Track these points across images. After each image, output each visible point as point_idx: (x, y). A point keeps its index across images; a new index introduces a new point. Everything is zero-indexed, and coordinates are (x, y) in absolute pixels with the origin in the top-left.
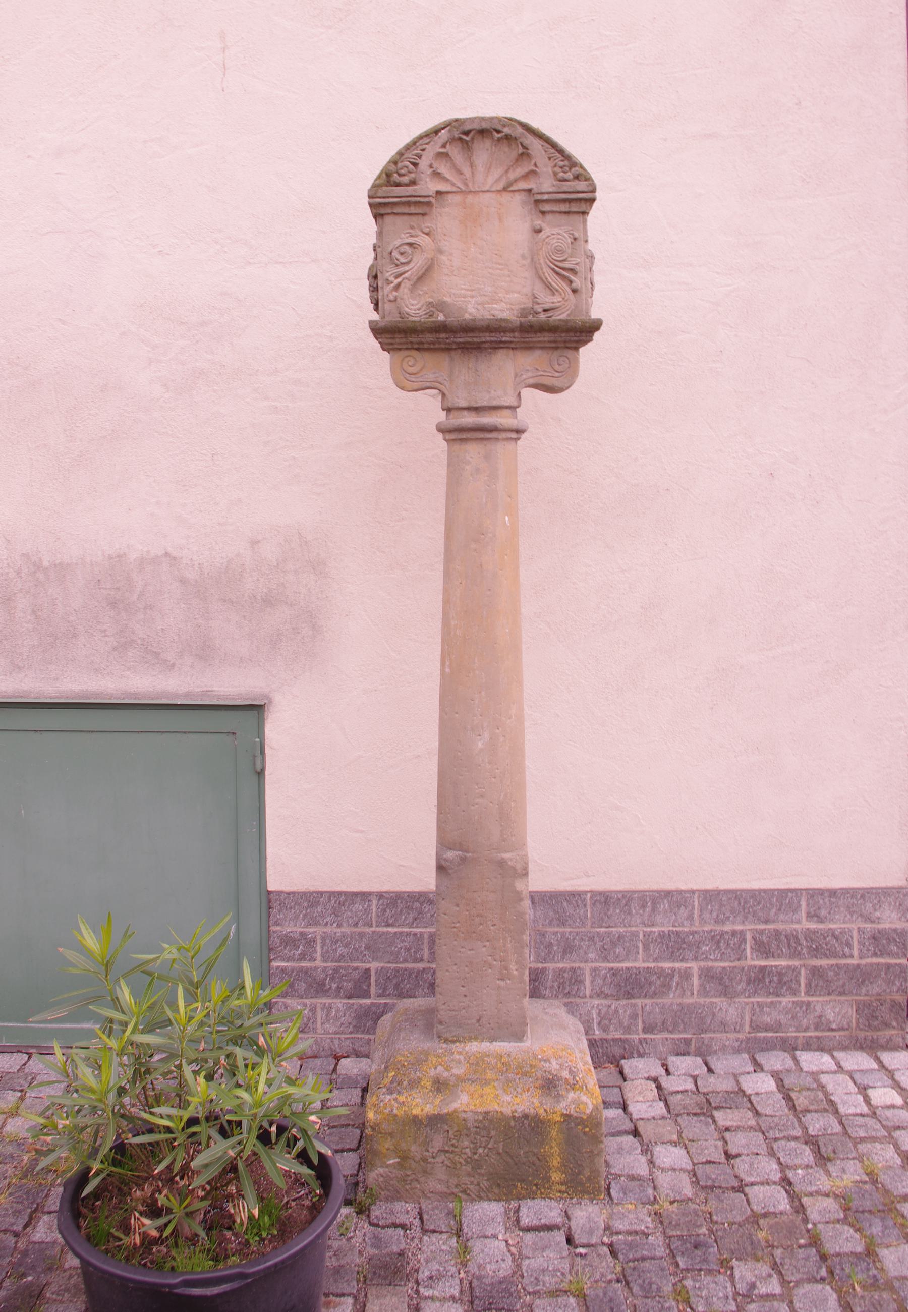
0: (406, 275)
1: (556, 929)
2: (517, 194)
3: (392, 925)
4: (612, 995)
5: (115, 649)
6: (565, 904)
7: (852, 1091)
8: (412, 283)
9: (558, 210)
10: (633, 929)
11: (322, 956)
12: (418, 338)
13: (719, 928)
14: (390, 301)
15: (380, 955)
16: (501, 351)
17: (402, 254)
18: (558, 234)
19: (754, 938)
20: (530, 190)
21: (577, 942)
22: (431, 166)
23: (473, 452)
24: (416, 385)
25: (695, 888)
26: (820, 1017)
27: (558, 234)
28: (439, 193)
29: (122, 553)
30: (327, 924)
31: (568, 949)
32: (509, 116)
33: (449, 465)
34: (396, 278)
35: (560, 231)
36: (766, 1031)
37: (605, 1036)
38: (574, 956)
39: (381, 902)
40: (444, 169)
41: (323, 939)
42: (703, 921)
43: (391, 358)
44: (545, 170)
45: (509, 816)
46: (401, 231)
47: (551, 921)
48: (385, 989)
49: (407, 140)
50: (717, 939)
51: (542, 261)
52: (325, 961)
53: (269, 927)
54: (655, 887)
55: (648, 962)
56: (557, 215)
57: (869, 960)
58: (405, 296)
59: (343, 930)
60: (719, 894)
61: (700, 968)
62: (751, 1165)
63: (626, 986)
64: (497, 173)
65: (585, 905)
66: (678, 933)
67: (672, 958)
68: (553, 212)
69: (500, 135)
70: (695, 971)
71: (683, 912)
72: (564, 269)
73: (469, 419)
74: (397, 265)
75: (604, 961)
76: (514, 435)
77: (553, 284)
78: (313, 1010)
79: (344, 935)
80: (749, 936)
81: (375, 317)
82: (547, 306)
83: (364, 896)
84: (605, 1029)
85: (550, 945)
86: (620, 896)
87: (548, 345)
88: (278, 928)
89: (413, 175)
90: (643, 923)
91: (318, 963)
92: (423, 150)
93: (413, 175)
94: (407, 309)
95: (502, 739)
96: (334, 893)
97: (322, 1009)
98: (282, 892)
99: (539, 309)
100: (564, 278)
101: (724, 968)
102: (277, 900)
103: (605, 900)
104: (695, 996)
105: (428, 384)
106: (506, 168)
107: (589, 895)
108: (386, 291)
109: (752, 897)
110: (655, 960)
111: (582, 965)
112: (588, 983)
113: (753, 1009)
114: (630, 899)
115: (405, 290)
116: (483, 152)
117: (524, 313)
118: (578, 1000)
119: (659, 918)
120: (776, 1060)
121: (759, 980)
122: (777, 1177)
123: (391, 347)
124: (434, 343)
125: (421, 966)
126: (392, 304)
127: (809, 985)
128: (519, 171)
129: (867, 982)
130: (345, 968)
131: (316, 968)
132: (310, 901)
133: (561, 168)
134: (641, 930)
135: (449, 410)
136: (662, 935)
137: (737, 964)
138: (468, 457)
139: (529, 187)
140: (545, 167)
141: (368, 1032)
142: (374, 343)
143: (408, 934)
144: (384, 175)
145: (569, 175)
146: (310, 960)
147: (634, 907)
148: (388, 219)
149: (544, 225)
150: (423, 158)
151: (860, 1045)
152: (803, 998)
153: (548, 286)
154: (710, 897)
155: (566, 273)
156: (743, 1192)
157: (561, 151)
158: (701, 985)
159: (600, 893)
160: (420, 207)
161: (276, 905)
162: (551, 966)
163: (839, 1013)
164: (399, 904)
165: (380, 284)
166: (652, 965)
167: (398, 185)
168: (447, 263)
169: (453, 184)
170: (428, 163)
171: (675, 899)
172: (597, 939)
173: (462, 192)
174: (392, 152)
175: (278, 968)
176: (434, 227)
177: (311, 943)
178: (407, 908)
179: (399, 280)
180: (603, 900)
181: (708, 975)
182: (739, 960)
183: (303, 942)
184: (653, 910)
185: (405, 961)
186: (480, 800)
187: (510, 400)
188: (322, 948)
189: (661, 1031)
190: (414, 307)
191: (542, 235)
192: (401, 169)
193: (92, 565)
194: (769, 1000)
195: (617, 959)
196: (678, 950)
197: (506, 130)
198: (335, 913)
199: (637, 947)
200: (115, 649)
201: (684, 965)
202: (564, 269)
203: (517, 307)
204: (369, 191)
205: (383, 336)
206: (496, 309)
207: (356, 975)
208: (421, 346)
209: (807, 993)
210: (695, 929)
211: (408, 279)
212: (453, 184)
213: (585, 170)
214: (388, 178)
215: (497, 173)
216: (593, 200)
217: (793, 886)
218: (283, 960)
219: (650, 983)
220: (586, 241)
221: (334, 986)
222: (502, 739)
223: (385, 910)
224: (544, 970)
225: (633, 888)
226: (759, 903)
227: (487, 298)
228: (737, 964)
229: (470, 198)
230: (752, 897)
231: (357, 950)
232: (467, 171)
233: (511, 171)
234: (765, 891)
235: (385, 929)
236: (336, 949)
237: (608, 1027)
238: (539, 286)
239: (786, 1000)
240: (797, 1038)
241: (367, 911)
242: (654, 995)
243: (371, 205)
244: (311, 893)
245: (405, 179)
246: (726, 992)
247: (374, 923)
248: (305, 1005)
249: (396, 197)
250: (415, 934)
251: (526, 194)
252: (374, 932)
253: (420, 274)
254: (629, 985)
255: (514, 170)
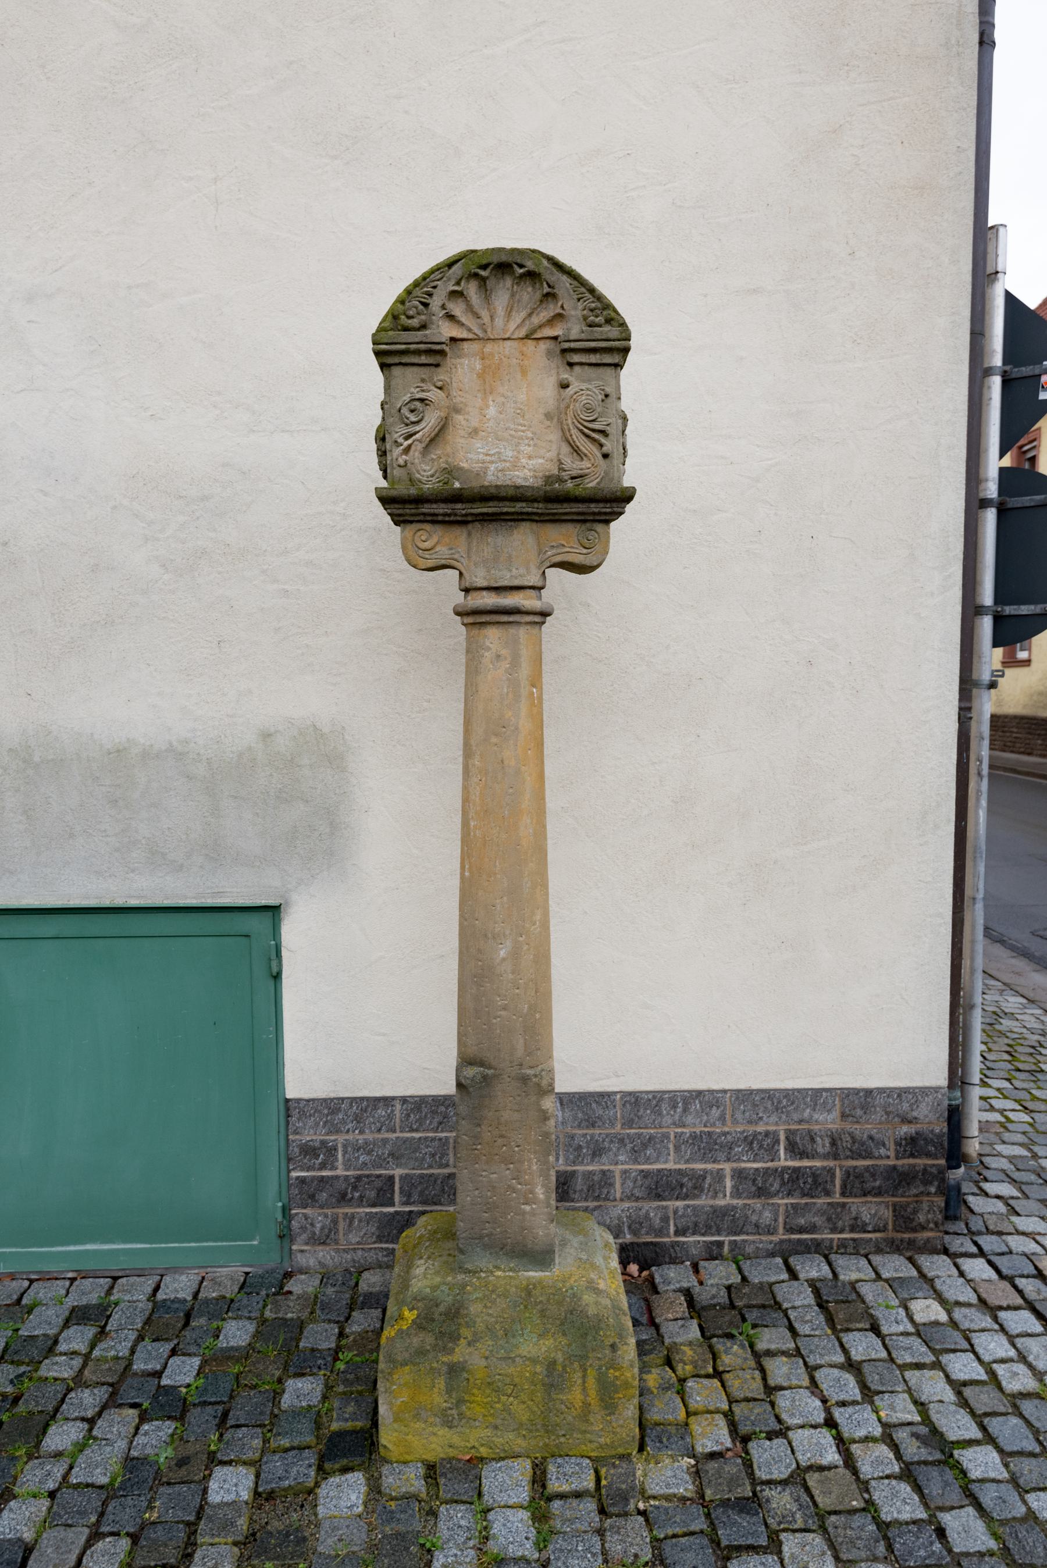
0: (417, 436)
1: (585, 1132)
2: (541, 343)
3: (417, 1130)
4: (642, 1198)
5: (117, 850)
6: (594, 1105)
7: (946, 1399)
8: (424, 445)
9: (588, 361)
10: (664, 1130)
11: (344, 1164)
12: (428, 507)
13: (751, 1129)
14: (399, 466)
15: (403, 1161)
16: (524, 524)
17: (412, 411)
18: (588, 389)
19: (787, 1138)
20: (555, 338)
21: (606, 1144)
22: (443, 307)
23: (493, 637)
24: (430, 563)
25: (727, 1087)
26: (856, 1219)
27: (588, 389)
28: (453, 340)
29: (272, 730)
30: (348, 1131)
31: (597, 1152)
32: (532, 248)
33: (467, 652)
34: (406, 439)
35: (590, 387)
36: (801, 1233)
37: (636, 1240)
38: (604, 1159)
39: (405, 1106)
40: (457, 309)
41: (345, 1146)
42: (735, 1122)
43: (402, 532)
44: (573, 313)
45: (536, 1025)
46: (410, 382)
47: (580, 1123)
48: (409, 1196)
49: (417, 274)
50: (749, 1141)
51: (570, 421)
52: (347, 1170)
53: (288, 1135)
54: (686, 1087)
55: (679, 1163)
56: (586, 367)
57: (906, 1161)
58: (416, 461)
59: (365, 1137)
60: (751, 1094)
61: (733, 1170)
62: (794, 1401)
63: (657, 1188)
64: (518, 317)
65: (615, 1106)
66: (709, 1134)
67: (703, 1159)
68: (581, 364)
69: (521, 271)
70: (728, 1173)
71: (715, 1113)
72: (594, 430)
73: (489, 600)
74: (407, 425)
75: (634, 1164)
76: (537, 619)
77: (581, 448)
78: (335, 1221)
79: (366, 1143)
80: (782, 1137)
81: (384, 484)
82: (574, 473)
83: (387, 1101)
84: (635, 1233)
85: (580, 1147)
86: (650, 1097)
87: (575, 517)
88: (297, 1137)
89: (423, 317)
90: (674, 1124)
91: (340, 1172)
92: (435, 287)
93: (423, 317)
94: (418, 476)
95: (525, 947)
96: (355, 1098)
97: (344, 1219)
98: (301, 1100)
99: (565, 475)
100: (594, 440)
101: (757, 1169)
102: (295, 1108)
103: (634, 1100)
104: (728, 1198)
105: (443, 562)
106: (529, 311)
107: (618, 1096)
108: (395, 454)
109: (785, 1097)
110: (687, 1162)
111: (612, 1168)
112: (618, 1186)
113: (787, 1211)
114: (661, 1099)
115: (415, 453)
116: (503, 292)
117: (549, 479)
118: (609, 1204)
119: (689, 1119)
120: (813, 1268)
121: (793, 1181)
122: (820, 1417)
123: (401, 519)
124: (449, 515)
125: (446, 1171)
126: (402, 470)
127: (844, 1186)
128: (544, 315)
129: (903, 1183)
130: (368, 1176)
131: (337, 1177)
132: (330, 1108)
133: (592, 310)
134: (672, 1132)
135: (467, 591)
136: (694, 1137)
137: (770, 1164)
138: (488, 644)
139: (556, 334)
140: (575, 310)
141: (392, 1242)
142: (382, 516)
143: (433, 1139)
144: (390, 316)
145: (600, 319)
146: (331, 1169)
147: (665, 1107)
148: (397, 371)
149: (571, 379)
150: (435, 298)
151: (895, 1247)
152: (837, 1198)
153: (576, 451)
154: (743, 1096)
155: (597, 435)
156: (786, 1437)
157: (592, 290)
158: (733, 1187)
159: (630, 1093)
160: (435, 355)
161: (295, 1113)
162: (579, 1168)
163: (875, 1214)
164: (423, 1108)
165: (388, 447)
166: (683, 1167)
167: (406, 329)
168: (463, 422)
169: (470, 330)
170: (440, 304)
171: (706, 1098)
172: (627, 1141)
173: (483, 339)
174: (398, 289)
175: (297, 1178)
176: (448, 380)
177: (332, 1151)
178: (432, 1112)
179: (410, 441)
180: (633, 1100)
181: (739, 1175)
182: (772, 1161)
183: (324, 1150)
184: (685, 1110)
185: (430, 1167)
186: (503, 1013)
187: (533, 580)
188: (344, 1155)
189: (694, 1234)
190: (426, 473)
191: (570, 391)
192: (409, 309)
193: (89, 760)
194: (803, 1201)
195: (648, 1160)
196: (710, 1151)
197: (530, 265)
198: (358, 1119)
199: (668, 1149)
200: (117, 850)
201: (717, 1166)
202: (594, 430)
203: (541, 474)
204: (374, 335)
205: (392, 506)
206: (518, 477)
207: (378, 1183)
208: (435, 518)
209: (843, 1194)
210: (726, 1129)
211: (420, 441)
212: (470, 330)
213: (618, 314)
214: (395, 319)
215: (518, 317)
216: (626, 350)
217: (827, 1086)
218: (302, 1170)
219: (682, 1185)
220: (619, 398)
221: (357, 1195)
222: (525, 947)
223: (408, 1115)
224: (573, 1173)
225: (664, 1088)
226: (793, 1103)
227: (508, 464)
228: (770, 1164)
229: (489, 348)
230: (785, 1097)
231: (380, 1158)
232: (485, 314)
233: (534, 315)
234: (799, 1091)
235: (409, 1135)
236: (358, 1158)
237: (639, 1230)
238: (566, 449)
239: (821, 1201)
240: (832, 1240)
241: (390, 1117)
242: (686, 1197)
243: (378, 354)
244: (332, 1100)
245: (415, 322)
246: (762, 1192)
247: (398, 1128)
248: (326, 1216)
249: (406, 344)
250: (440, 1139)
251: (552, 342)
252: (397, 1138)
253: (433, 434)
254: (661, 1187)
255: (538, 314)
